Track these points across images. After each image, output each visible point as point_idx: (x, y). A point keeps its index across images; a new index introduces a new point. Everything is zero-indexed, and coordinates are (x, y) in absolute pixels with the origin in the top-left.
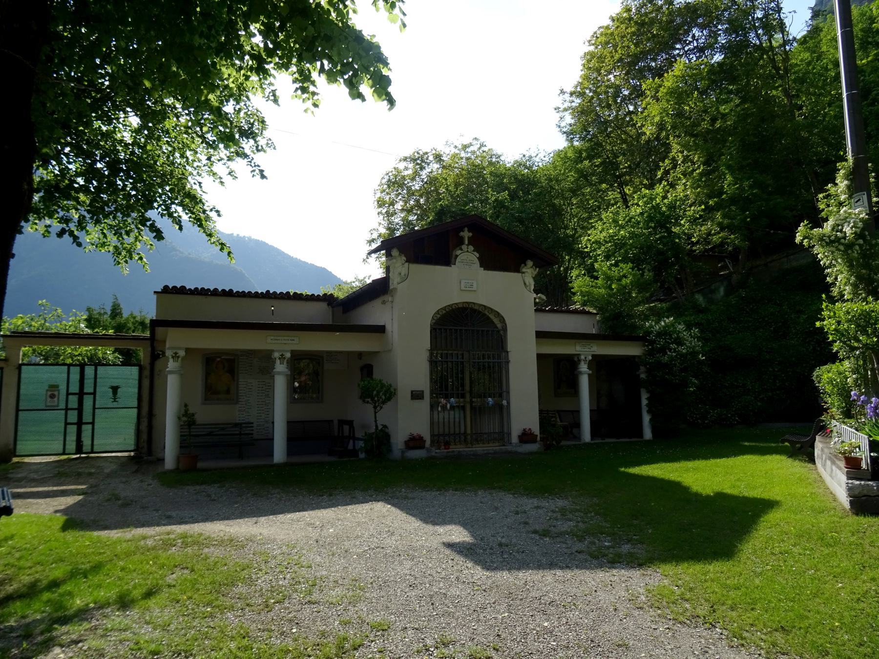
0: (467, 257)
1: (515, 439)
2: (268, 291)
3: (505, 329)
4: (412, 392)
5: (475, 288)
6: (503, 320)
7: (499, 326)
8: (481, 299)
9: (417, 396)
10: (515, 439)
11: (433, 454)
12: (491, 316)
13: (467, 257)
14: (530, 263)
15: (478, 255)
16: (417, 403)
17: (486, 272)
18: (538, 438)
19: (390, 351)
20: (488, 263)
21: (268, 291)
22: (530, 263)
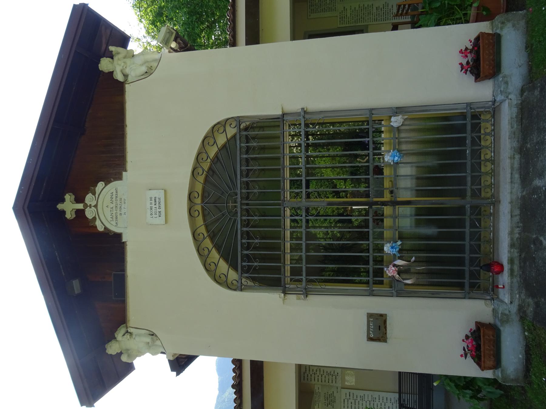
0: (109, 206)
1: (480, 92)
2: (233, 386)
3: (239, 120)
4: (370, 339)
5: (160, 194)
6: (222, 125)
7: (231, 131)
8: (178, 177)
9: (378, 328)
10: (480, 92)
11: (514, 309)
12: (213, 151)
13: (109, 206)
14: (105, 65)
15: (101, 185)
16: (393, 329)
17: (129, 165)
18: (484, 27)
19: (305, 112)
20: (110, 161)
21: (233, 386)
22: (105, 65)
